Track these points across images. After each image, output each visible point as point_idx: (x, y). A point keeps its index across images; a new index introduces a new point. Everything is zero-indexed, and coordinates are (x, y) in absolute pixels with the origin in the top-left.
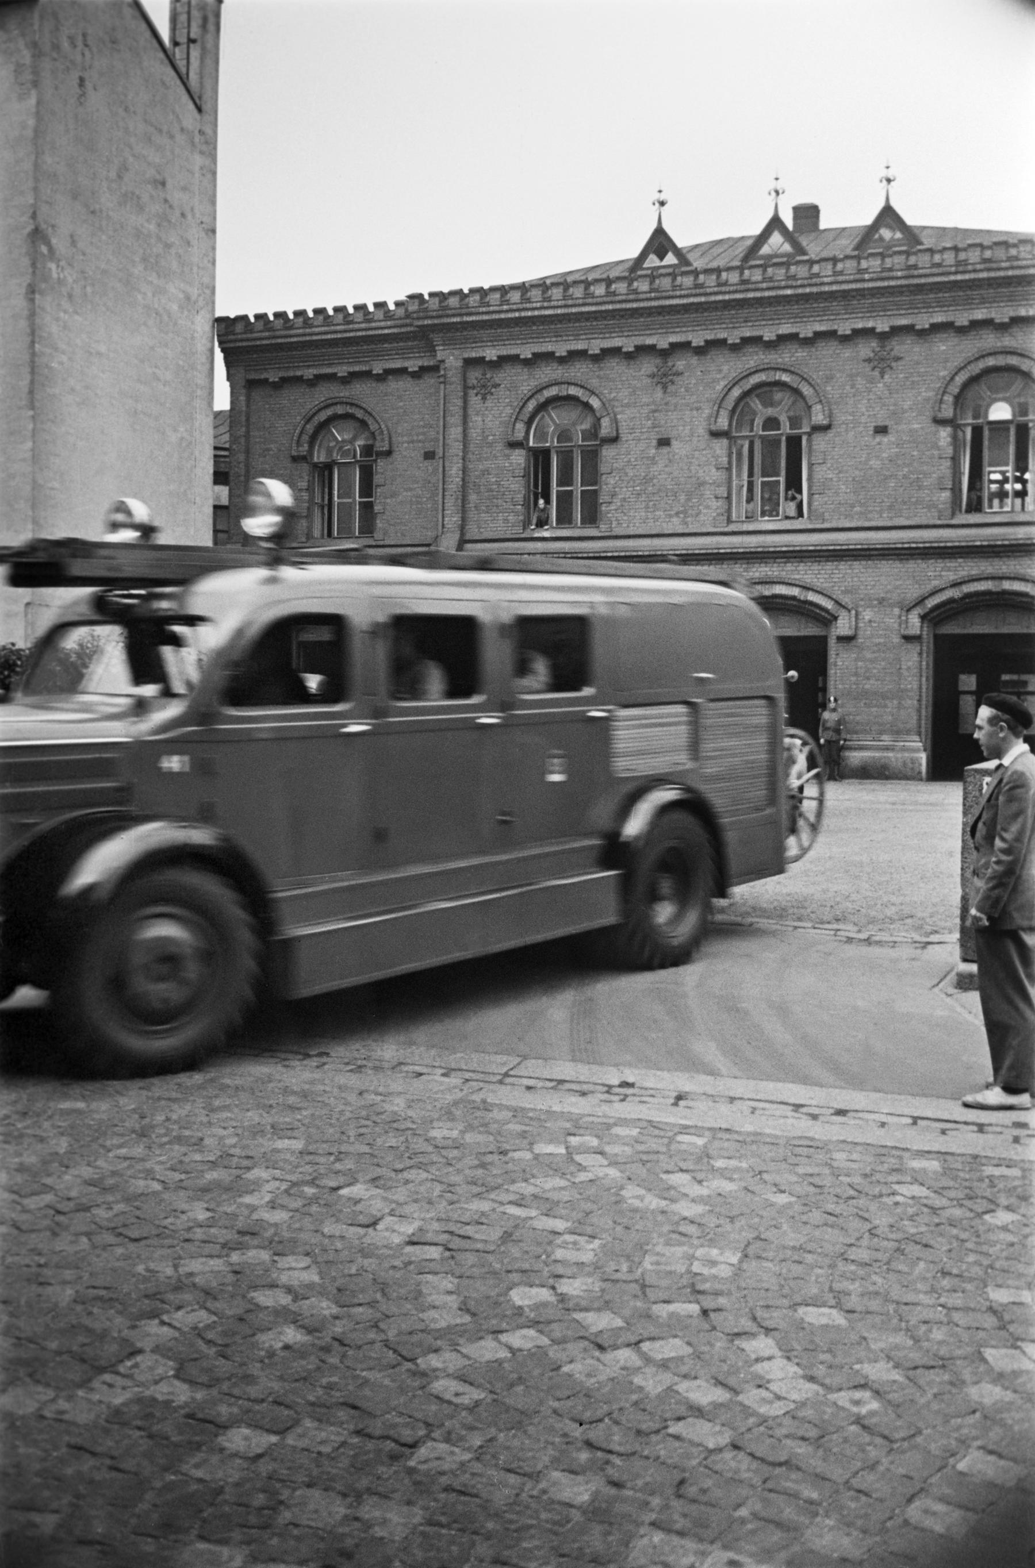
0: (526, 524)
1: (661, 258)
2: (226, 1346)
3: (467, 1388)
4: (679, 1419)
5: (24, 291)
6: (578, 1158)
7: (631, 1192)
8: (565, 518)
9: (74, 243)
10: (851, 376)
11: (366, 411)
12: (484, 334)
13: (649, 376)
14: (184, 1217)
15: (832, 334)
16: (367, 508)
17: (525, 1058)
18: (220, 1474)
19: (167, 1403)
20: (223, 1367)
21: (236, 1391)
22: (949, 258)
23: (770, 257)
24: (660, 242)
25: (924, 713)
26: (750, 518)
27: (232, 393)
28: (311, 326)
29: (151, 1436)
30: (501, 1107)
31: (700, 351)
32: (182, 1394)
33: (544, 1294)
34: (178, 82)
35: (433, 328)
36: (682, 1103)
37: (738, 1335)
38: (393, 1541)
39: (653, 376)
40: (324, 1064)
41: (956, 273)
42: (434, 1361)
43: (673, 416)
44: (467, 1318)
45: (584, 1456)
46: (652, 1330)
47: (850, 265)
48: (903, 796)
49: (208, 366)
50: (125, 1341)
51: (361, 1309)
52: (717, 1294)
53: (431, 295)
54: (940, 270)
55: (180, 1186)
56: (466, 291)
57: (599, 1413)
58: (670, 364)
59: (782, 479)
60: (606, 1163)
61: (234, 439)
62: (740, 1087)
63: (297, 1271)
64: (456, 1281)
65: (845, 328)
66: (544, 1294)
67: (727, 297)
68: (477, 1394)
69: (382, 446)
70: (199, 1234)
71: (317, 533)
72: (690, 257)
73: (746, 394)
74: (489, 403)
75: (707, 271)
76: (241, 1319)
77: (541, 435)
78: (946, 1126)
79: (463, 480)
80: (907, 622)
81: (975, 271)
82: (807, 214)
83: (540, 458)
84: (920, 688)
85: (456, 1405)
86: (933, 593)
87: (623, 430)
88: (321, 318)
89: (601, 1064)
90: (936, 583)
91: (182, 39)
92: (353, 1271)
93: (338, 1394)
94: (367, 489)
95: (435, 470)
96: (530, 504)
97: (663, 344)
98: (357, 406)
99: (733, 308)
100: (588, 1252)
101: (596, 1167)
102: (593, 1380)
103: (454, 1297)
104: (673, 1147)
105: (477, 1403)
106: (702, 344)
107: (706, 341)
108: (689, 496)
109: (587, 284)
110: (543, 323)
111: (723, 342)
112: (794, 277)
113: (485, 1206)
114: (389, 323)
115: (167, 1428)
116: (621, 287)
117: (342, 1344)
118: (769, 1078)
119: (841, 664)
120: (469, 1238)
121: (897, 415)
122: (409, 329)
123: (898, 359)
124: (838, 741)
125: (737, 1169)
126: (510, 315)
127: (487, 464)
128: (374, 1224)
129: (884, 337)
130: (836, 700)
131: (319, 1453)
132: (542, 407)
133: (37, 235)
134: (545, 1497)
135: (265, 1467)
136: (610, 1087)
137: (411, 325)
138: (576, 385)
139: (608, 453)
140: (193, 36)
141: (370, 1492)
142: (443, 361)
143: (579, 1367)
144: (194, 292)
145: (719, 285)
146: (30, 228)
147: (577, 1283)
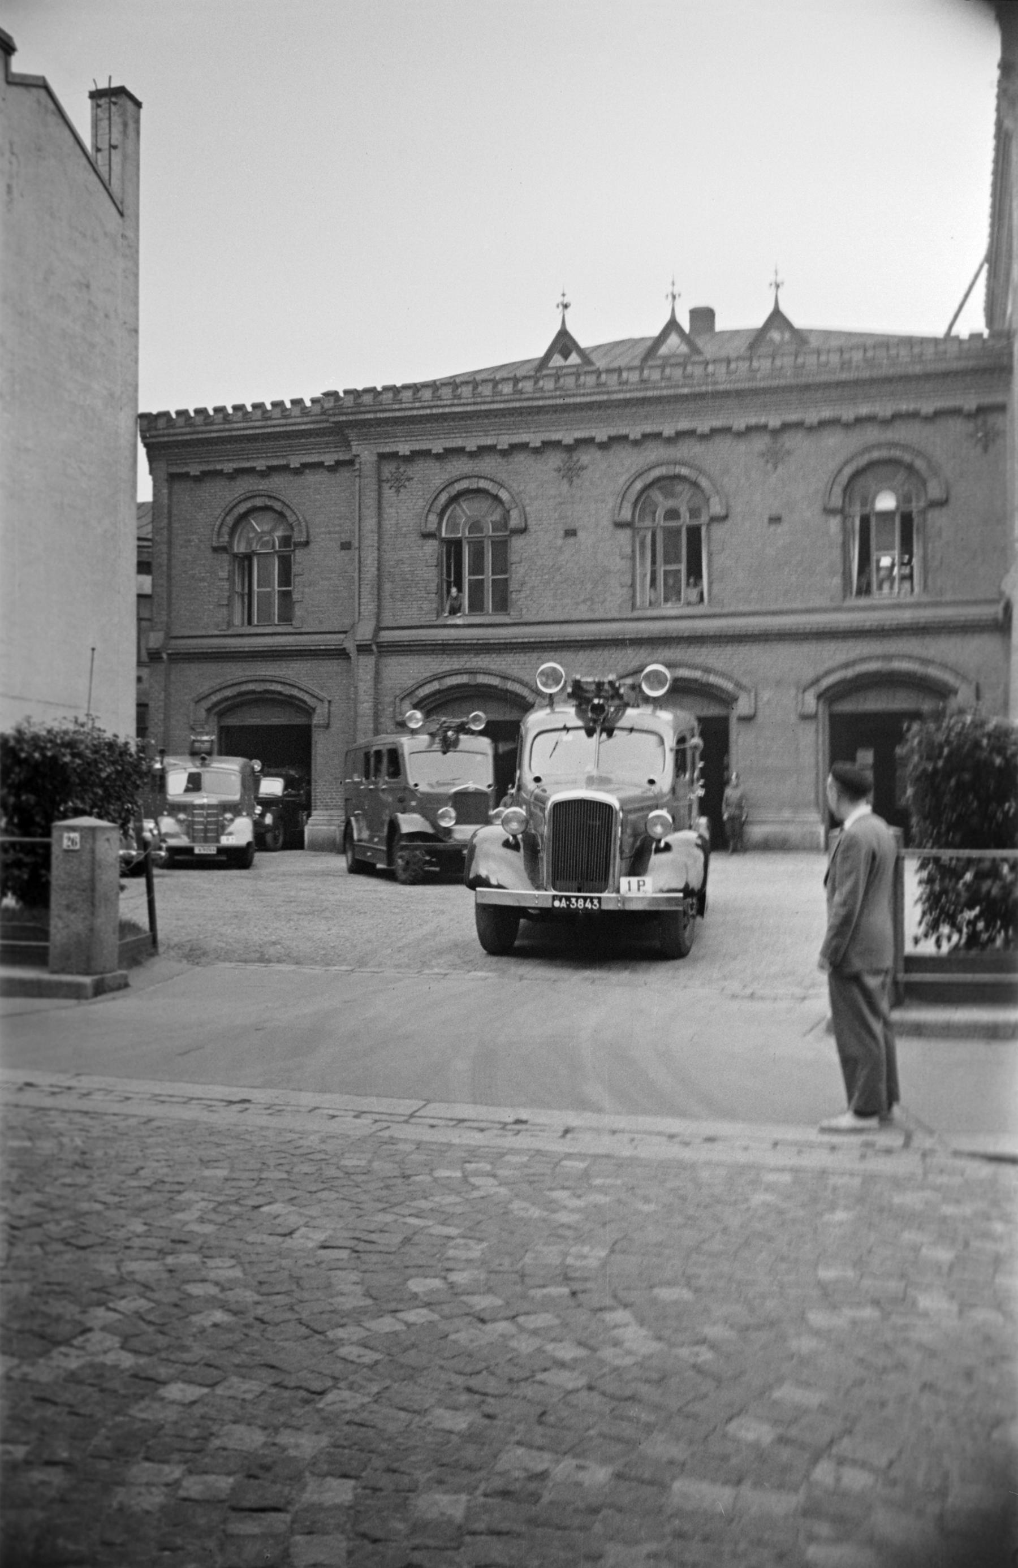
0: (439, 613)
2: (163, 1325)
3: (367, 1352)
4: (545, 1370)
6: (472, 1180)
7: (516, 1205)
8: (477, 606)
11: (284, 503)
12: (399, 429)
13: (555, 470)
14: (124, 1230)
15: (726, 430)
16: (286, 596)
17: (428, 1101)
18: (161, 1416)
19: (115, 1367)
20: (161, 1341)
21: (172, 1357)
22: (835, 359)
23: (666, 358)
24: (564, 343)
27: (155, 486)
29: (102, 1390)
30: (406, 1141)
31: (604, 446)
32: (127, 1360)
33: (437, 1283)
34: (101, 187)
35: (351, 424)
36: (569, 1136)
37: (601, 1309)
38: (305, 1459)
39: (559, 470)
40: (247, 1109)
42: (341, 1333)
44: (369, 1302)
45: (464, 1398)
46: (526, 1306)
47: (744, 366)
49: (131, 460)
50: (80, 1323)
51: (279, 1297)
52: (586, 1279)
53: (346, 392)
55: (119, 1206)
56: (379, 389)
57: (478, 1367)
58: (575, 459)
59: (683, 567)
60: (496, 1183)
61: (156, 531)
62: (622, 1122)
63: (223, 1269)
64: (361, 1275)
65: (739, 424)
66: (437, 1283)
68: (377, 1356)
69: (299, 537)
70: (137, 1242)
71: (237, 621)
72: (593, 357)
74: (402, 496)
75: (609, 371)
76: (176, 1305)
77: (453, 527)
78: (802, 1147)
79: (379, 569)
82: (703, 317)
83: (454, 547)
85: (359, 1364)
88: (240, 414)
89: (499, 1105)
91: (105, 146)
92: (272, 1269)
93: (259, 1358)
94: (286, 578)
95: (352, 560)
96: (442, 592)
97: (568, 439)
100: (476, 1251)
101: (487, 1186)
102: (475, 1344)
103: (359, 1287)
104: (558, 1170)
105: (377, 1362)
109: (495, 383)
110: (453, 420)
111: (624, 438)
113: (389, 1218)
114: (305, 419)
115: (116, 1384)
116: (527, 386)
117: (262, 1321)
118: (645, 1112)
119: (742, 744)
120: (373, 1242)
122: (324, 425)
125: (613, 1186)
126: (422, 412)
128: (291, 1233)
130: (737, 777)
131: (244, 1400)
132: (454, 499)
134: (430, 1427)
135: (198, 1410)
136: (506, 1124)
137: (327, 421)
138: (485, 478)
140: (114, 142)
141: (286, 1426)
143: (464, 1335)
147: (465, 1274)
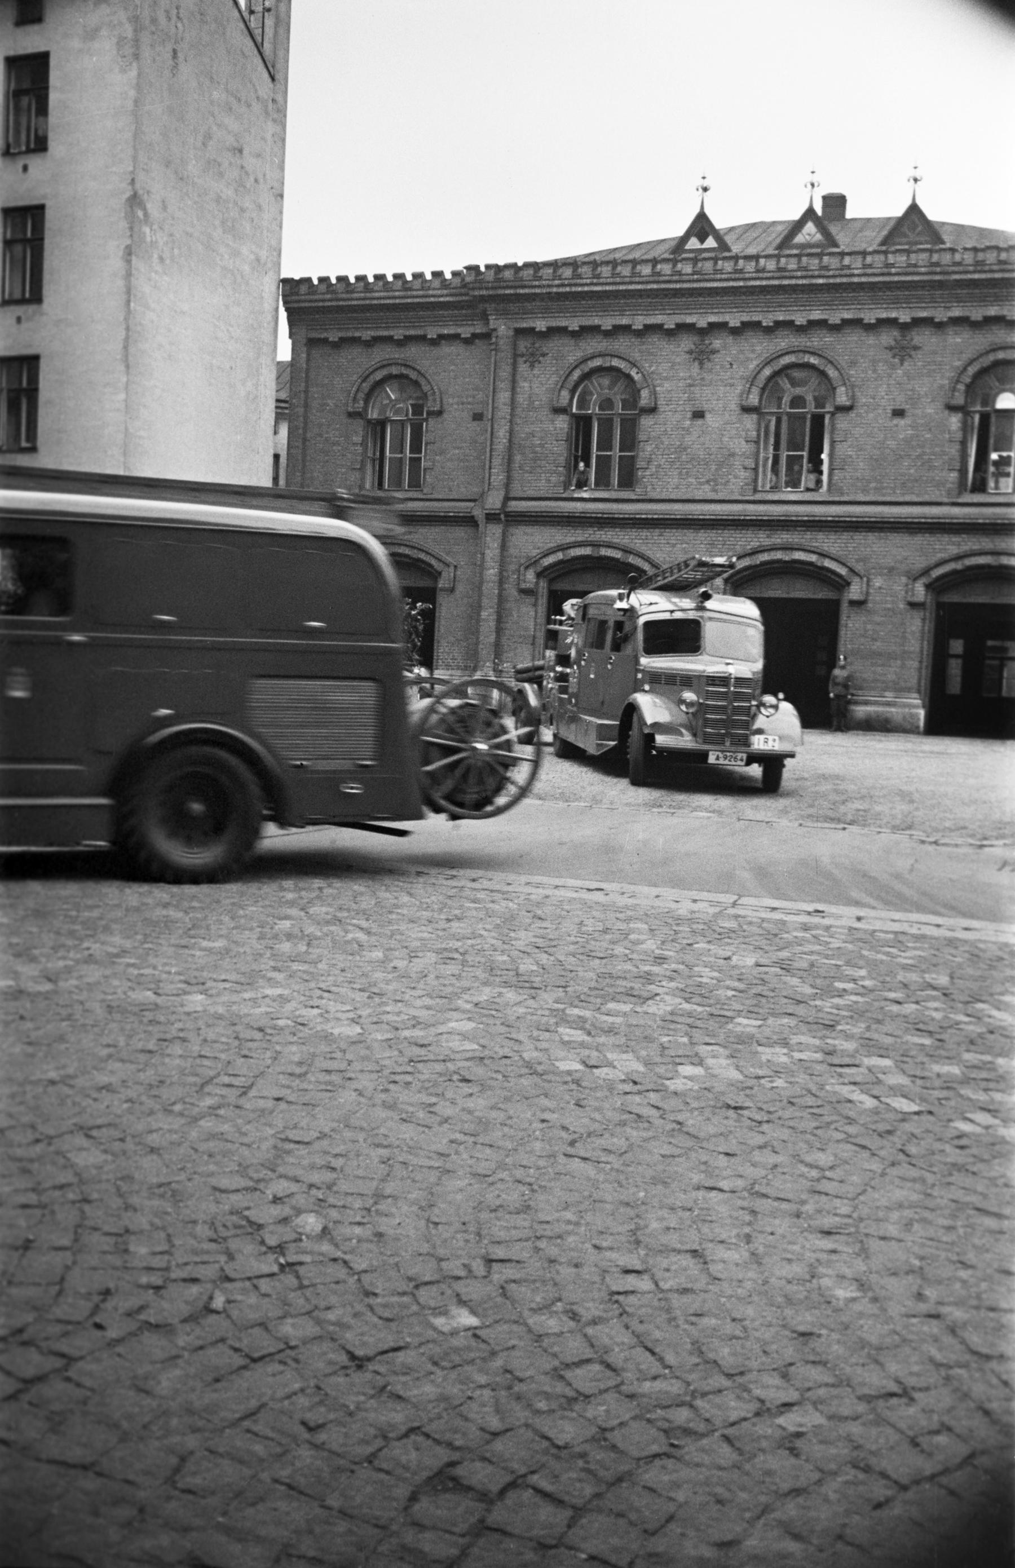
0: (566, 485)
1: (702, 241)
5: (121, 253)
8: (603, 481)
9: (165, 208)
10: (874, 362)
11: (419, 372)
16: (415, 462)
23: (802, 246)
24: (701, 226)
25: (924, 671)
26: (775, 488)
27: (293, 350)
28: (372, 291)
31: (736, 332)
39: (690, 352)
41: (974, 272)
43: (707, 391)
48: (909, 746)
54: (961, 268)
59: (805, 454)
61: (293, 394)
67: (764, 283)
72: (729, 239)
73: (776, 374)
74: (536, 372)
77: (583, 403)
80: (913, 589)
81: (992, 271)
82: (836, 203)
83: (582, 424)
84: (922, 651)
86: (938, 565)
87: (661, 402)
88: (381, 283)
90: (940, 556)
96: (571, 467)
97: (702, 323)
98: (414, 369)
99: (769, 293)
106: (738, 325)
107: (742, 323)
108: (720, 465)
109: (614, 264)
112: (826, 268)
114: (445, 292)
116: (666, 269)
121: (914, 400)
123: (916, 348)
124: (845, 696)
127: (533, 427)
129: (905, 327)
130: (845, 658)
132: (586, 376)
133: (135, 201)
139: (646, 422)
142: (495, 330)
144: (264, 254)
145: (758, 271)
146: (128, 194)
